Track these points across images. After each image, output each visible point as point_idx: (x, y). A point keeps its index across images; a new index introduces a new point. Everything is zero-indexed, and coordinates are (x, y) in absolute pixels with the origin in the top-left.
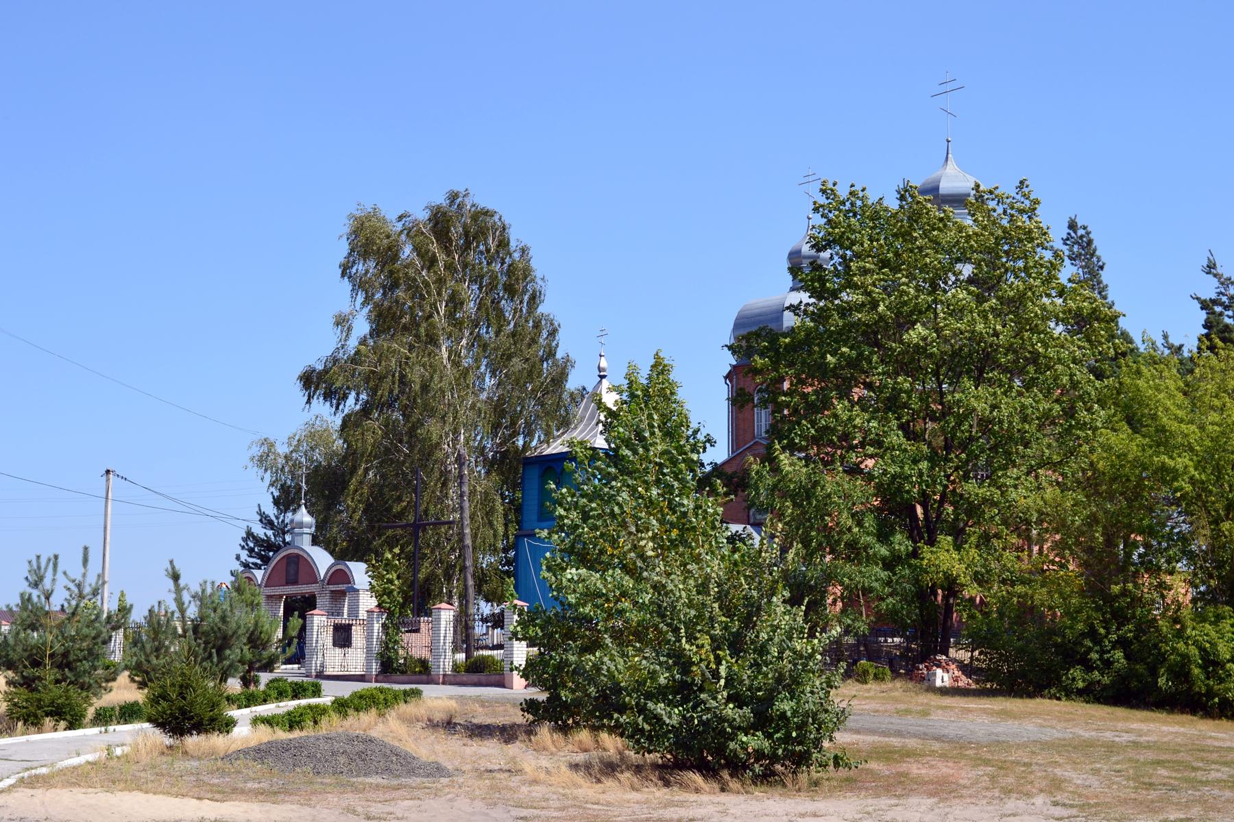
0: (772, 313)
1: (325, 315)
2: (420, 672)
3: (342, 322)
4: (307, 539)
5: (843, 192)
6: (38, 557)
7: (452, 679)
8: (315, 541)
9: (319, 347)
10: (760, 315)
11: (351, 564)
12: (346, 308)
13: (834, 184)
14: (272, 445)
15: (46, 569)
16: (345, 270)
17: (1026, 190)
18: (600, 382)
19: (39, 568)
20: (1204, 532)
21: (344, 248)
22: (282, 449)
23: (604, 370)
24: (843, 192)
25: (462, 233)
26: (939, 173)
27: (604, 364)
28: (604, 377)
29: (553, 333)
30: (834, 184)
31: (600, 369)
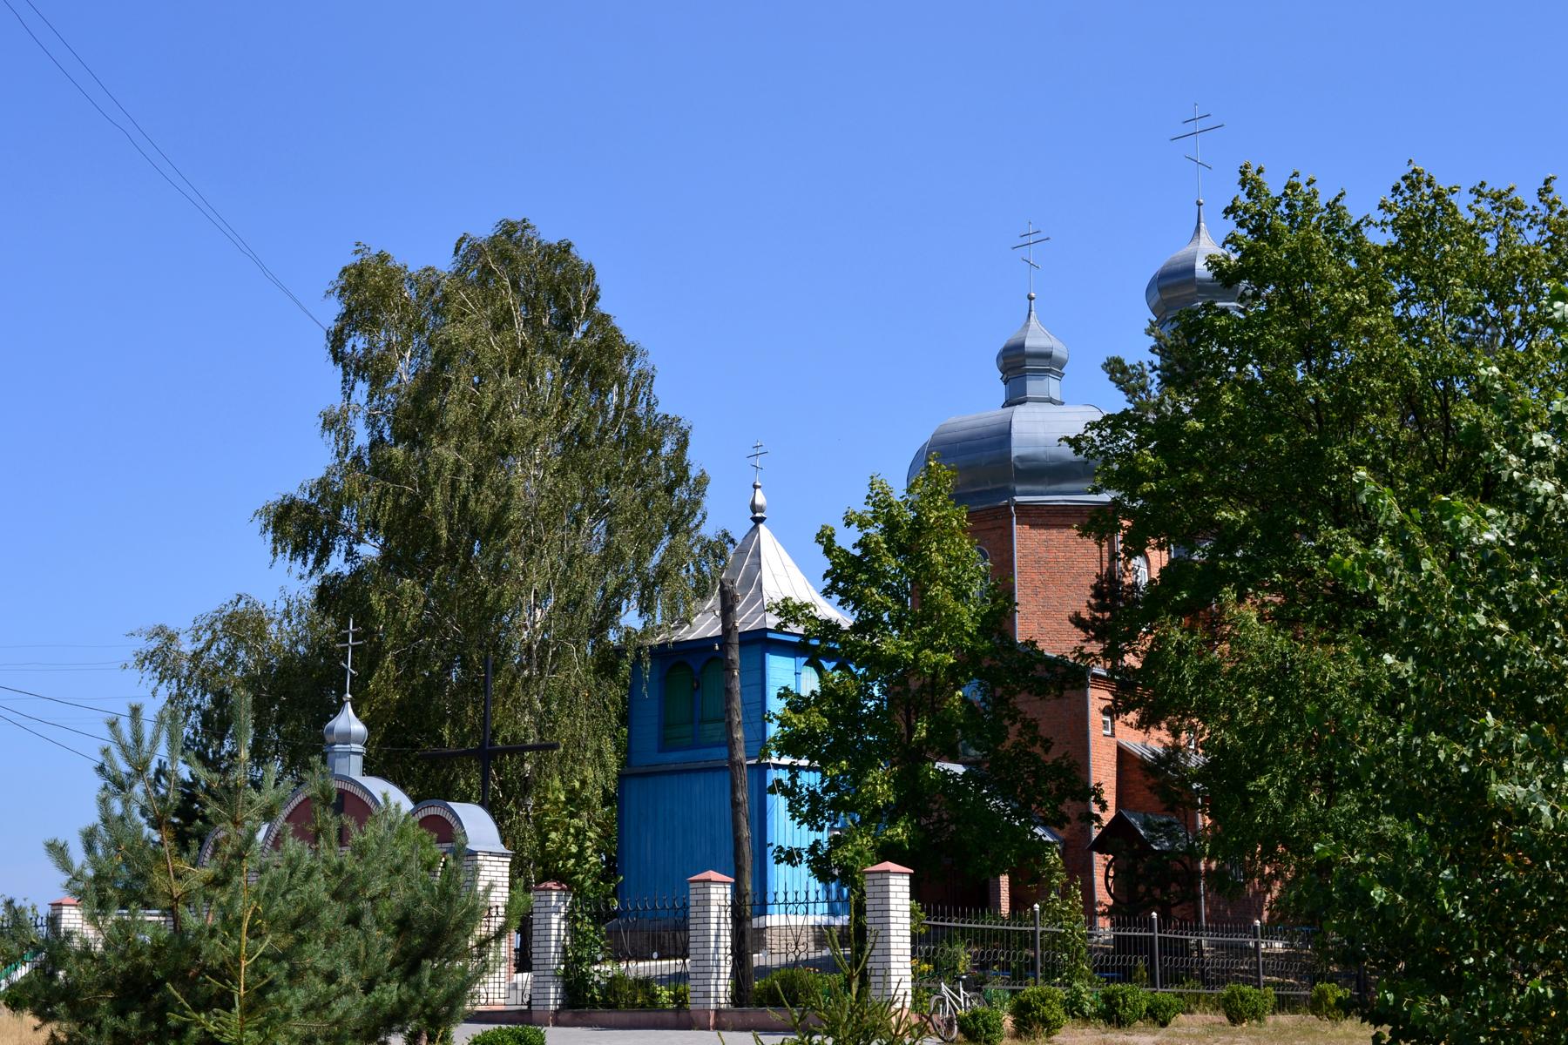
0: (990, 435)
1: (296, 424)
2: (643, 1006)
3: (332, 422)
4: (356, 763)
5: (1275, 187)
6: (135, 712)
7: (738, 1019)
8: (369, 769)
9: (306, 464)
10: (969, 439)
11: (457, 807)
12: (336, 401)
13: (1260, 171)
14: (171, 638)
15: (154, 743)
16: (336, 341)
17: (1550, 197)
18: (756, 528)
19: (138, 740)
20: (251, 866)
21: (336, 307)
22: (187, 646)
23: (761, 509)
24: (1275, 187)
25: (535, 288)
26: (1190, 248)
27: (760, 499)
28: (762, 520)
29: (683, 444)
30: (1260, 171)
31: (754, 508)
